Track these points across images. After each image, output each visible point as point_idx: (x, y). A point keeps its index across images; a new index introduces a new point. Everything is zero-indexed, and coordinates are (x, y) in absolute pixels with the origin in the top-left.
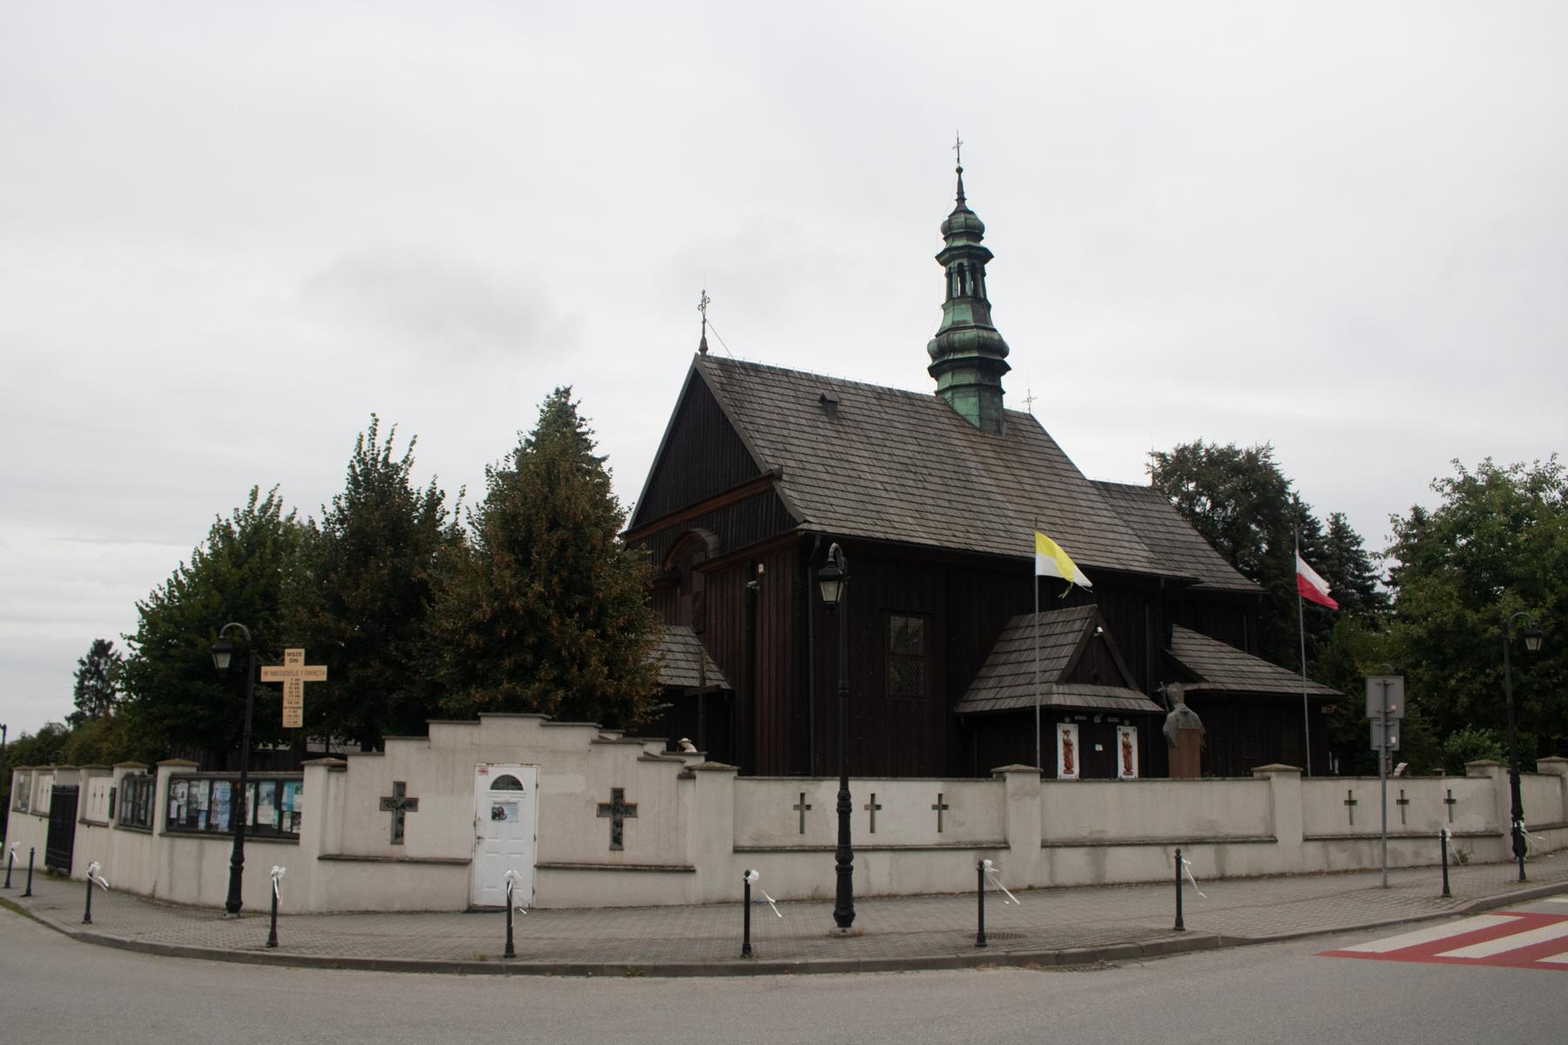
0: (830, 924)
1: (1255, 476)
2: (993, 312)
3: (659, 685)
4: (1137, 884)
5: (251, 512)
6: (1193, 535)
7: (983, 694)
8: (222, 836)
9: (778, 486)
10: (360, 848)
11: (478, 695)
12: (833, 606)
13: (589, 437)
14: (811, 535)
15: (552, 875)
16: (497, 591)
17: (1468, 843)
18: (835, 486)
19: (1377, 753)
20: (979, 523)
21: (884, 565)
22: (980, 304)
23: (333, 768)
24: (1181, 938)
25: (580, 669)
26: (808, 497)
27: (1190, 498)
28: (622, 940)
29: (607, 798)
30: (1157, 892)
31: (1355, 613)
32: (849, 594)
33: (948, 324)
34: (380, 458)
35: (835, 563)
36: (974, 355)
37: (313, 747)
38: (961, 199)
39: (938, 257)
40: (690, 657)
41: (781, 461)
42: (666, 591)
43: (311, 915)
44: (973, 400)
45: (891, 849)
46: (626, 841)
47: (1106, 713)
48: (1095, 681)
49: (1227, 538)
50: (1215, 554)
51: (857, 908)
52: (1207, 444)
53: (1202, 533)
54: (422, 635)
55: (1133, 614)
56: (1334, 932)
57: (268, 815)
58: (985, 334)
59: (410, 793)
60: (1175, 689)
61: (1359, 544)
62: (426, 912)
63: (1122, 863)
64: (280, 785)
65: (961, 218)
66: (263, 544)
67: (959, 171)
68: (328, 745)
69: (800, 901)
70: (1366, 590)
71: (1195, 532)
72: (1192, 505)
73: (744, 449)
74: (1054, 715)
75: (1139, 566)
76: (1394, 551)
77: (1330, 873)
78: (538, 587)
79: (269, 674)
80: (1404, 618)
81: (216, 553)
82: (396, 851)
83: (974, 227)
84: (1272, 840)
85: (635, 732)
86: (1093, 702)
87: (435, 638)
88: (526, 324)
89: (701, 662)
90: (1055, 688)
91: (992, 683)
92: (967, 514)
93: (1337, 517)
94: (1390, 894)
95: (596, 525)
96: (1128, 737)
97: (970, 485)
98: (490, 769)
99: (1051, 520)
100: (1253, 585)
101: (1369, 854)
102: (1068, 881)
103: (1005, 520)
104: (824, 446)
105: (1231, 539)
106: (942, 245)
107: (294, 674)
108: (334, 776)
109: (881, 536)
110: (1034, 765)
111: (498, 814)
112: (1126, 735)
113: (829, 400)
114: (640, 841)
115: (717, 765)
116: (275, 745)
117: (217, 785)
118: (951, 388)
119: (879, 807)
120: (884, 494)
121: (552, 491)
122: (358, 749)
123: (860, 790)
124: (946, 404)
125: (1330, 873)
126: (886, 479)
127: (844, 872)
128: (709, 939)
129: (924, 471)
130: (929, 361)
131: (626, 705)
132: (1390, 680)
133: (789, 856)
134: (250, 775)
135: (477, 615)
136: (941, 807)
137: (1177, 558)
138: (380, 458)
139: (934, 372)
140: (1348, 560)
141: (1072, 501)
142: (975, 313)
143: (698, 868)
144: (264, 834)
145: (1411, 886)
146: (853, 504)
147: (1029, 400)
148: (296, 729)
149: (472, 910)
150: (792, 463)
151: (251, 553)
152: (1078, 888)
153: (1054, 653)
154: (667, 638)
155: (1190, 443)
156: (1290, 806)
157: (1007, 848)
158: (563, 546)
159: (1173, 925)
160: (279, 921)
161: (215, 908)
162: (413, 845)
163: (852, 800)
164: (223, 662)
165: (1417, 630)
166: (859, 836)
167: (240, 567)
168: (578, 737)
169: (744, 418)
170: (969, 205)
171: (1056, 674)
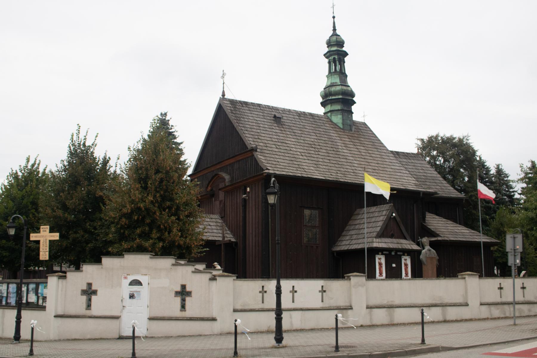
0: (273, 342)
1: (462, 148)
3: (203, 240)
4: (408, 324)
5: (27, 167)
6: (435, 174)
7: (344, 243)
8: (12, 307)
9: (255, 154)
10: (72, 312)
11: (125, 245)
12: (273, 205)
13: (175, 133)
16: (133, 200)
18: (280, 154)
19: (510, 267)
20: (342, 169)
21: (297, 187)
22: (343, 75)
23: (60, 277)
24: (424, 347)
25: (169, 233)
26: (268, 159)
27: (434, 158)
28: (183, 350)
29: (179, 289)
30: (229, 336)
31: (506, 206)
32: (280, 199)
33: (329, 84)
34: (82, 143)
35: (274, 187)
36: (340, 97)
37: (56, 268)
38: (334, 30)
39: (324, 55)
40: (218, 228)
41: (257, 143)
42: (206, 200)
43: (51, 341)
44: (340, 116)
45: (302, 310)
46: (187, 307)
47: (397, 250)
48: (392, 236)
49: (450, 175)
50: (445, 182)
51: (284, 335)
52: (441, 135)
53: (439, 173)
54: (101, 219)
55: (409, 207)
56: (491, 344)
57: (32, 298)
58: (345, 88)
59: (94, 288)
60: (425, 240)
61: (508, 177)
62: (101, 339)
63: (401, 315)
64: (37, 285)
65: (334, 38)
66: (32, 181)
67: (334, 17)
68: (61, 267)
69: (262, 332)
70: (511, 197)
71: (436, 173)
72: (435, 161)
73: (241, 138)
74: (374, 252)
76: (522, 179)
77: (491, 319)
78: (151, 198)
79: (34, 237)
80: (526, 209)
81: (11, 185)
82: (88, 313)
83: (340, 42)
84: (467, 305)
85: (192, 260)
86: (391, 246)
87: (106, 221)
89: (222, 230)
90: (375, 240)
91: (348, 238)
92: (337, 166)
93: (498, 166)
94: (517, 328)
95: (176, 171)
96: (406, 261)
97: (338, 153)
98: (128, 277)
99: (373, 168)
100: (462, 195)
101: (508, 310)
102: (379, 323)
103: (353, 168)
104: (275, 137)
105: (453, 175)
106: (326, 50)
107: (45, 237)
108: (61, 280)
109: (300, 175)
110: (364, 273)
111: (132, 296)
112: (405, 260)
113: (278, 117)
114: (194, 307)
115: (226, 274)
116: (39, 268)
117: (10, 285)
118: (330, 111)
119: (296, 292)
120: (301, 157)
121: (156, 157)
122: (74, 269)
123: (286, 284)
124: (328, 118)
125: (491, 319)
126: (302, 151)
127: (279, 320)
128: (221, 349)
129: (319, 147)
130: (321, 100)
131: (189, 249)
132: (516, 235)
133: (258, 313)
134: (24, 281)
135: (125, 210)
136: (323, 291)
137: (428, 184)
138: (82, 143)
139: (323, 104)
140: (503, 184)
141: (383, 160)
142: (340, 79)
143: (218, 318)
144: (30, 306)
145: (526, 324)
147: (364, 116)
148: (46, 261)
149: (121, 338)
150: (261, 144)
151: (27, 185)
152: (382, 326)
153: (374, 225)
154: (208, 220)
155: (434, 134)
156: (473, 289)
157: (352, 309)
158: (161, 181)
159: (420, 342)
160: (35, 344)
161: (10, 339)
162: (95, 310)
163: (282, 289)
164: (12, 232)
165: (531, 214)
166: (285, 304)
167: (22, 191)
168: (167, 262)
169: (241, 125)
170: (338, 32)
171: (375, 234)
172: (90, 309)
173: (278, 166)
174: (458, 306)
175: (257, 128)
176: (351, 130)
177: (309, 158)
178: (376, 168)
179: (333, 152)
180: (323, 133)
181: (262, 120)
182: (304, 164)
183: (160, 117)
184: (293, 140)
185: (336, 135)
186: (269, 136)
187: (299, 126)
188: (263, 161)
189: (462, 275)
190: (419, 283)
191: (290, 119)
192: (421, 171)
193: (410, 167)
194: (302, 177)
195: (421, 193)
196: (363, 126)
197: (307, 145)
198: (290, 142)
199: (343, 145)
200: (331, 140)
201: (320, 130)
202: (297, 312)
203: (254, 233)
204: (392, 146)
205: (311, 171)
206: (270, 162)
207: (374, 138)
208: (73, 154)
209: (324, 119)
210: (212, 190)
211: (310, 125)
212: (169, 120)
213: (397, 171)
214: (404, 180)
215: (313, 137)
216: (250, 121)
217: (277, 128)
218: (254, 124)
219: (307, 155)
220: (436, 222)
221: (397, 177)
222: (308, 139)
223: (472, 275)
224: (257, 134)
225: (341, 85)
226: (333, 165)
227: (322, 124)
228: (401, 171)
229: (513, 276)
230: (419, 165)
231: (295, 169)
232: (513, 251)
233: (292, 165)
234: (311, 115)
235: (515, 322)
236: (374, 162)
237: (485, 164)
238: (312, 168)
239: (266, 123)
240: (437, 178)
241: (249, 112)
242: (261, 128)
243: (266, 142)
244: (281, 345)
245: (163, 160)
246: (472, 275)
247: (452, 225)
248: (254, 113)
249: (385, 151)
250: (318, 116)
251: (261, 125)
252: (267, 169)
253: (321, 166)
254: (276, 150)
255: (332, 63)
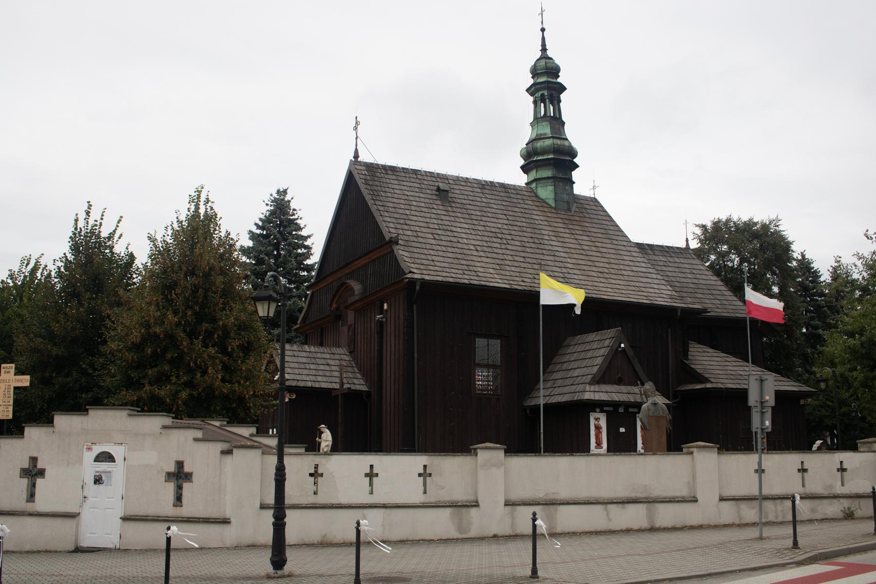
0: (270, 569)
1: (767, 239)
2: (567, 128)
3: (285, 388)
13: (298, 221)
14: (413, 282)
15: (132, 525)
17: (857, 501)
18: (439, 248)
22: (557, 122)
26: (416, 256)
27: (722, 255)
29: (172, 468)
33: (534, 136)
38: (544, 49)
39: (527, 90)
45: (385, 506)
46: (184, 500)
48: (619, 382)
58: (559, 142)
62: (47, 551)
65: (543, 63)
67: (543, 30)
74: (581, 410)
82: (30, 507)
83: (552, 69)
86: (616, 397)
88: (234, 147)
90: (588, 388)
97: (542, 247)
98: (93, 447)
99: (600, 270)
103: (564, 270)
104: (435, 221)
109: (466, 282)
111: (98, 480)
113: (443, 190)
118: (535, 180)
120: (475, 253)
124: (532, 191)
129: (509, 237)
130: (522, 162)
136: (425, 474)
137: (699, 296)
139: (525, 169)
146: (449, 260)
147: (594, 188)
149: (78, 550)
155: (724, 218)
157: (478, 506)
162: (41, 504)
168: (153, 423)
170: (549, 53)
172: (34, 502)
173: (431, 268)
174: (678, 501)
175: (407, 207)
176: (569, 210)
177: (489, 255)
178: (606, 270)
179: (533, 245)
180: (519, 214)
181: (416, 194)
182: (478, 264)
183: (276, 196)
184: (466, 226)
185: (542, 218)
186: (424, 220)
187: (479, 204)
188: (406, 259)
189: (688, 447)
190: (623, 463)
191: (466, 193)
192: (689, 276)
193: (670, 269)
194: (470, 284)
195: (679, 311)
196: (591, 203)
197: (490, 234)
198: (459, 230)
199: (551, 233)
200: (532, 226)
201: (517, 209)
202: (375, 511)
203: (393, 378)
204: (636, 235)
205: (489, 275)
206: (419, 261)
207: (608, 223)
208: (75, 248)
209: (526, 193)
210: (338, 309)
211: (499, 202)
212: (289, 201)
213: (642, 275)
214: (652, 290)
215: (500, 221)
216: (396, 196)
217: (441, 207)
218: (402, 201)
219: (486, 249)
220: (707, 358)
221: (641, 285)
222: (492, 225)
223: (708, 447)
224: (405, 217)
225: (552, 137)
226: (530, 266)
227: (520, 201)
228: (649, 275)
229: (759, 451)
230: (687, 266)
231: (461, 272)
232: (758, 404)
233: (456, 266)
234: (503, 186)
235: (761, 534)
236: (603, 260)
237: (812, 265)
238: (492, 271)
239: (422, 200)
240: (715, 287)
241: (396, 182)
242: (413, 208)
243: (418, 229)
244: (280, 572)
245: (201, 255)
246: (708, 447)
247: (734, 364)
248: (405, 183)
249: (625, 243)
250: (515, 188)
251: (414, 203)
252: (411, 272)
253: (508, 268)
254: (433, 242)
255: (539, 102)
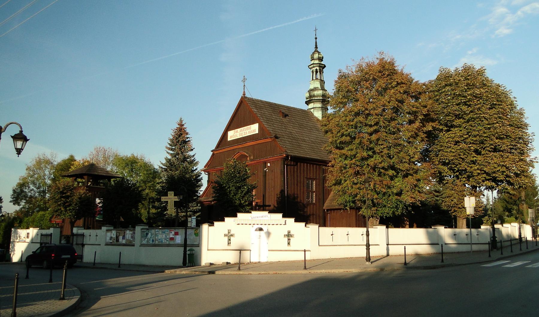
38: (316, 47)
46: (291, 243)
67: (316, 38)
75: (252, 126)
